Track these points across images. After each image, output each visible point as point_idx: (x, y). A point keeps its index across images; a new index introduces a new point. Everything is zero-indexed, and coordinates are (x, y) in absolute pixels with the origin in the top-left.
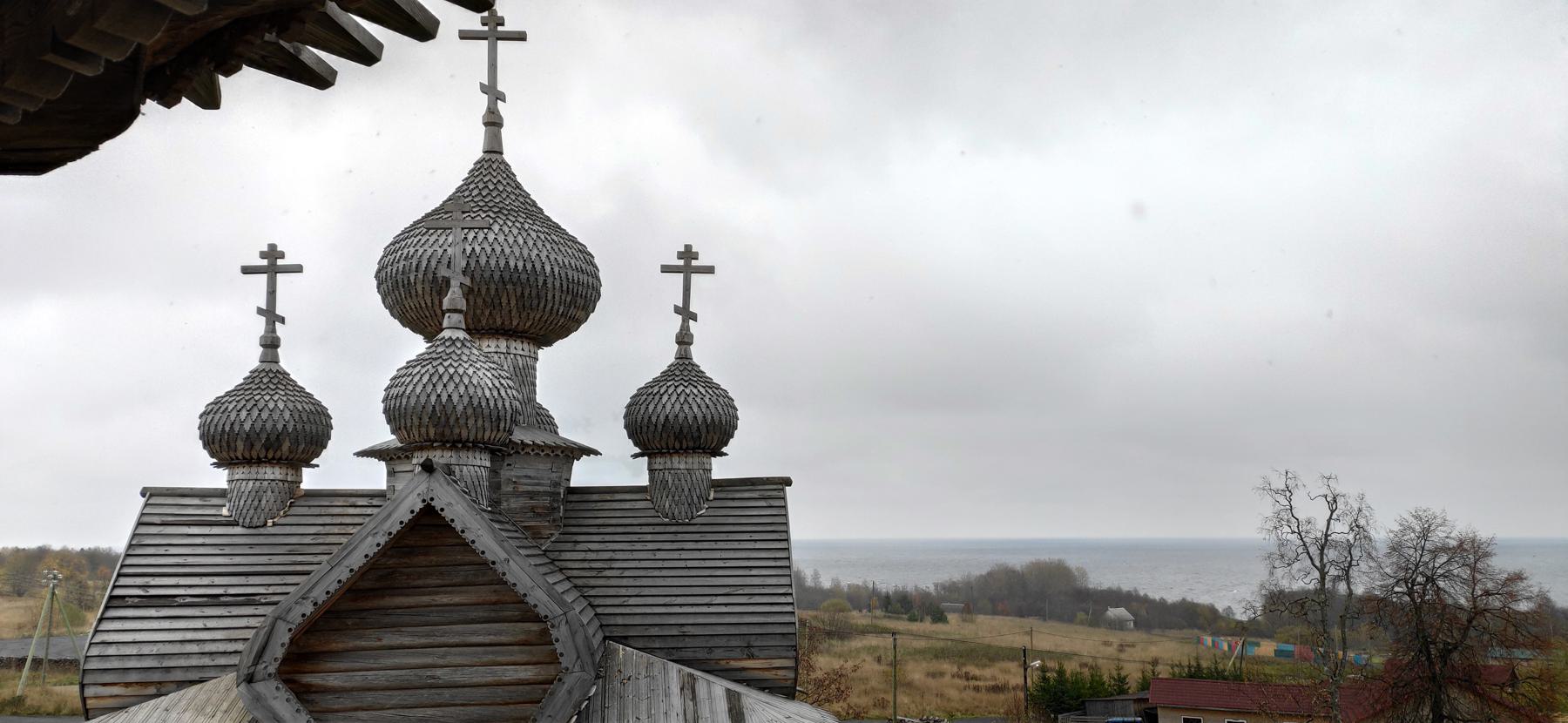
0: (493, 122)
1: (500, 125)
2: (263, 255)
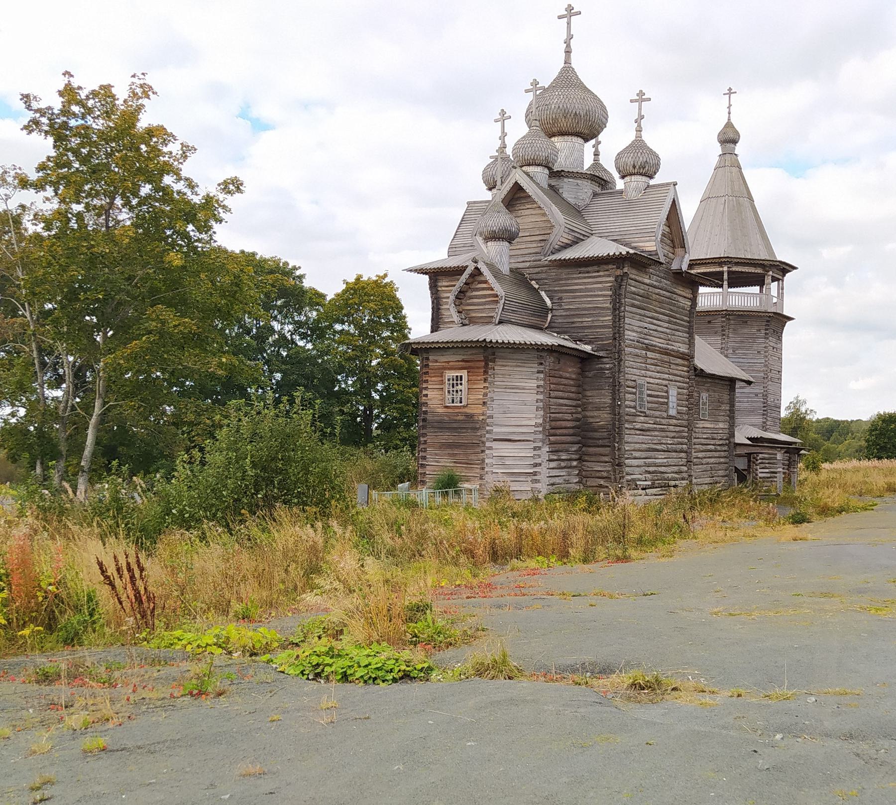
0: (568, 52)
1: (735, 142)
2: (638, 95)
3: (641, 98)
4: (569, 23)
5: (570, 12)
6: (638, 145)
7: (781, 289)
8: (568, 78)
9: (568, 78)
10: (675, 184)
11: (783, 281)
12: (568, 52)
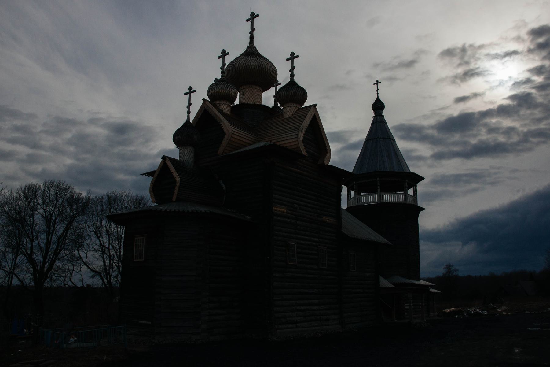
0: (252, 38)
2: (291, 55)
3: (293, 56)
4: (252, 23)
5: (254, 16)
6: (292, 84)
7: (415, 191)
8: (251, 51)
9: (251, 51)
10: (315, 105)
11: (416, 187)
12: (252, 38)
